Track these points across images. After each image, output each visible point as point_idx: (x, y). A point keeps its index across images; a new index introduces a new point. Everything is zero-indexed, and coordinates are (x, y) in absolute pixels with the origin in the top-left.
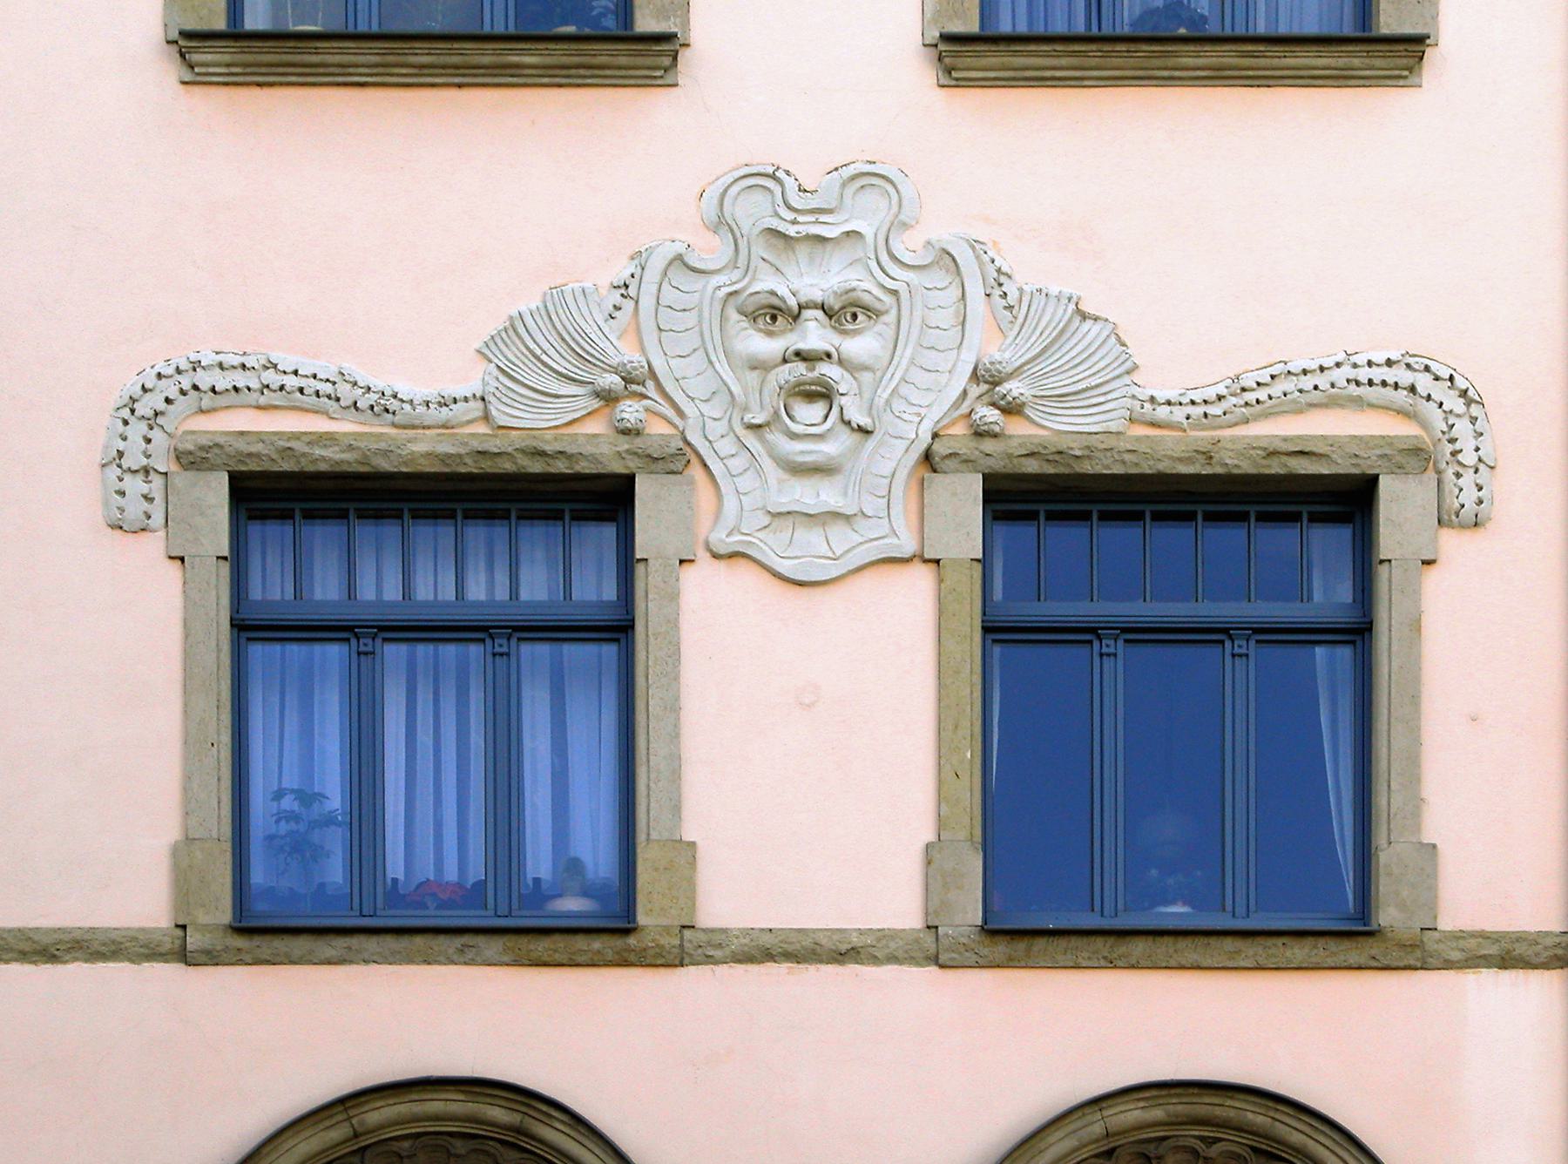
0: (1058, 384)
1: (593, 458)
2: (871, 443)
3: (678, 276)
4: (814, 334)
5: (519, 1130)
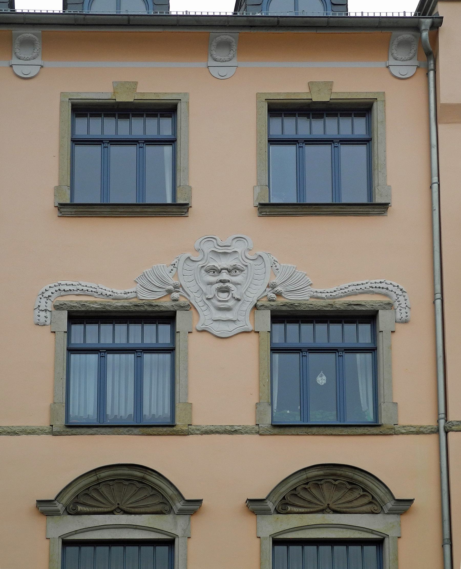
0: (290, 288)
2: (240, 303)
3: (189, 262)
5: (143, 478)
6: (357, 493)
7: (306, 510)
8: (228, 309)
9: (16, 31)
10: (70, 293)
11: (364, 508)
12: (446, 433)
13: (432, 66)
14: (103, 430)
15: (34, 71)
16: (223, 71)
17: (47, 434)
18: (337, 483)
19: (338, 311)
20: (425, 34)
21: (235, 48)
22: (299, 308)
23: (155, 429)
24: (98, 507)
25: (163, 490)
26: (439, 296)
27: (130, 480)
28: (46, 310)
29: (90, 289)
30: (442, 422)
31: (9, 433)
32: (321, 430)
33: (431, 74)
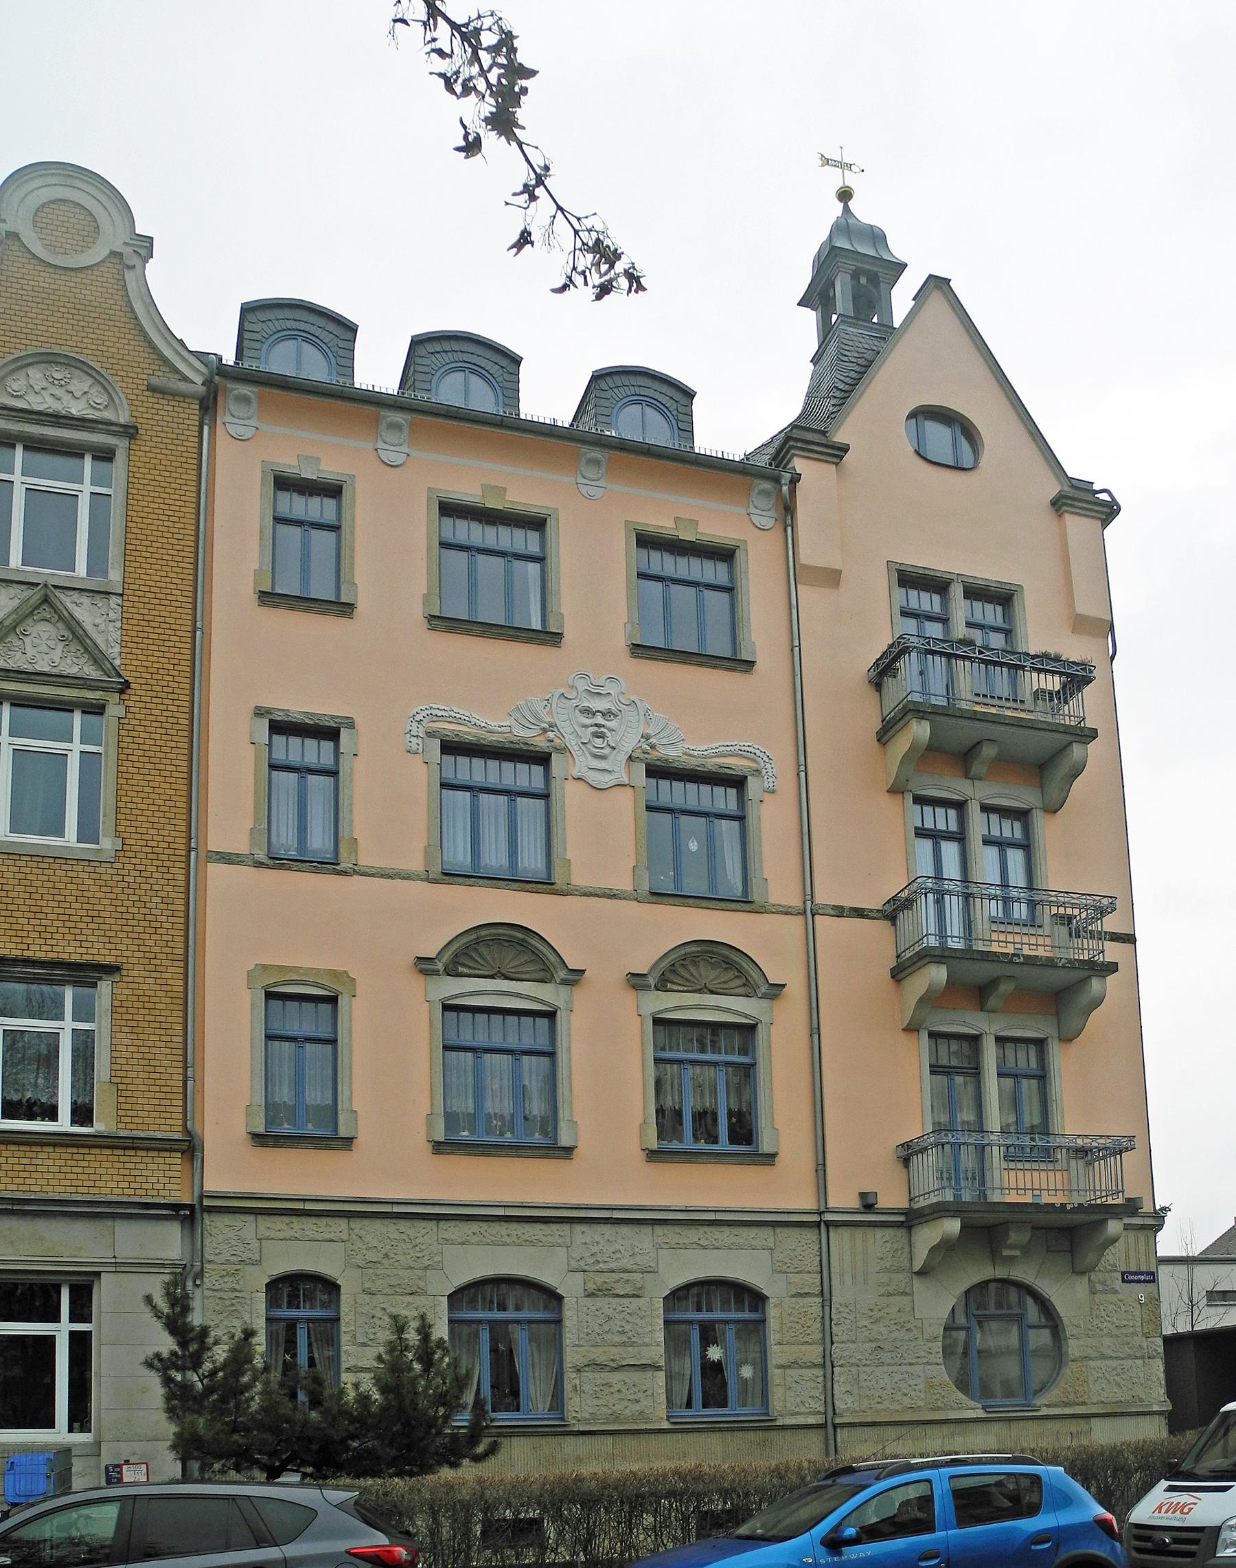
0: (665, 741)
1: (541, 747)
2: (615, 751)
3: (562, 699)
4: (599, 719)
5: (523, 940)
6: (731, 974)
7: (685, 989)
8: (603, 757)
9: (385, 413)
10: (441, 719)
11: (739, 991)
12: (813, 916)
13: (789, 522)
14: (481, 882)
15: (400, 459)
16: (593, 491)
17: (422, 880)
18: (713, 960)
19: (709, 772)
20: (785, 489)
21: (604, 467)
22: (672, 765)
23: (533, 885)
24: (475, 969)
25: (545, 955)
26: (803, 768)
27: (510, 941)
28: (417, 736)
29: (463, 717)
30: (809, 903)
31: (382, 876)
32: (697, 902)
33: (789, 529)
